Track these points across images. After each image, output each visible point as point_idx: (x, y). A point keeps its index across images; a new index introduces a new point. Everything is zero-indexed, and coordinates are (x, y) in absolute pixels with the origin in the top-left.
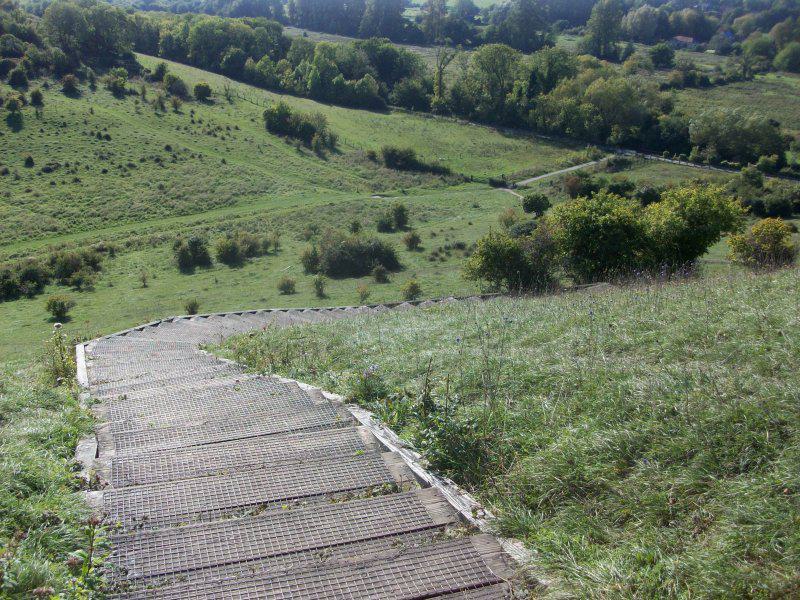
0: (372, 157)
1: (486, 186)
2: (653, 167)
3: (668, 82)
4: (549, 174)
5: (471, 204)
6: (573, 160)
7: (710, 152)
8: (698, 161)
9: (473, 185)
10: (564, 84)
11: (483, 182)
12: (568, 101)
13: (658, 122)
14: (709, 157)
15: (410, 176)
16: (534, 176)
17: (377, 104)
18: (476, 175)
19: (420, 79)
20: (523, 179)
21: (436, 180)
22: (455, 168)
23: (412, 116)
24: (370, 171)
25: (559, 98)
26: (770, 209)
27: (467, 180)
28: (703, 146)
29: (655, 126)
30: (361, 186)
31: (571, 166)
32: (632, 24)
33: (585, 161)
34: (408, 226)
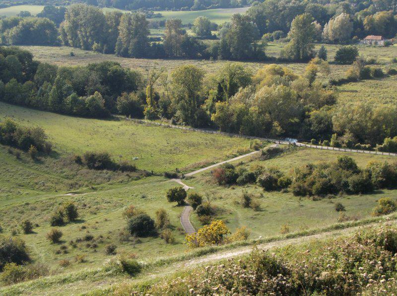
0: (78, 161)
1: (162, 178)
2: (300, 153)
3: (345, 78)
4: (218, 164)
5: (140, 196)
6: (238, 152)
7: (347, 137)
8: (337, 145)
9: (151, 178)
10: (241, 92)
11: (161, 175)
12: (240, 106)
13: (309, 117)
14: (346, 141)
15: (106, 173)
16: (202, 167)
17: (105, 113)
18: (157, 170)
19: (138, 93)
20: (194, 171)
21: (123, 176)
22: (140, 167)
23: (128, 123)
24: (72, 173)
25: (235, 103)
26: (354, 187)
27: (149, 175)
28: (340, 134)
29: (307, 120)
30: (61, 186)
31: (236, 156)
32: (332, 30)
33: (248, 152)
34: (79, 218)
